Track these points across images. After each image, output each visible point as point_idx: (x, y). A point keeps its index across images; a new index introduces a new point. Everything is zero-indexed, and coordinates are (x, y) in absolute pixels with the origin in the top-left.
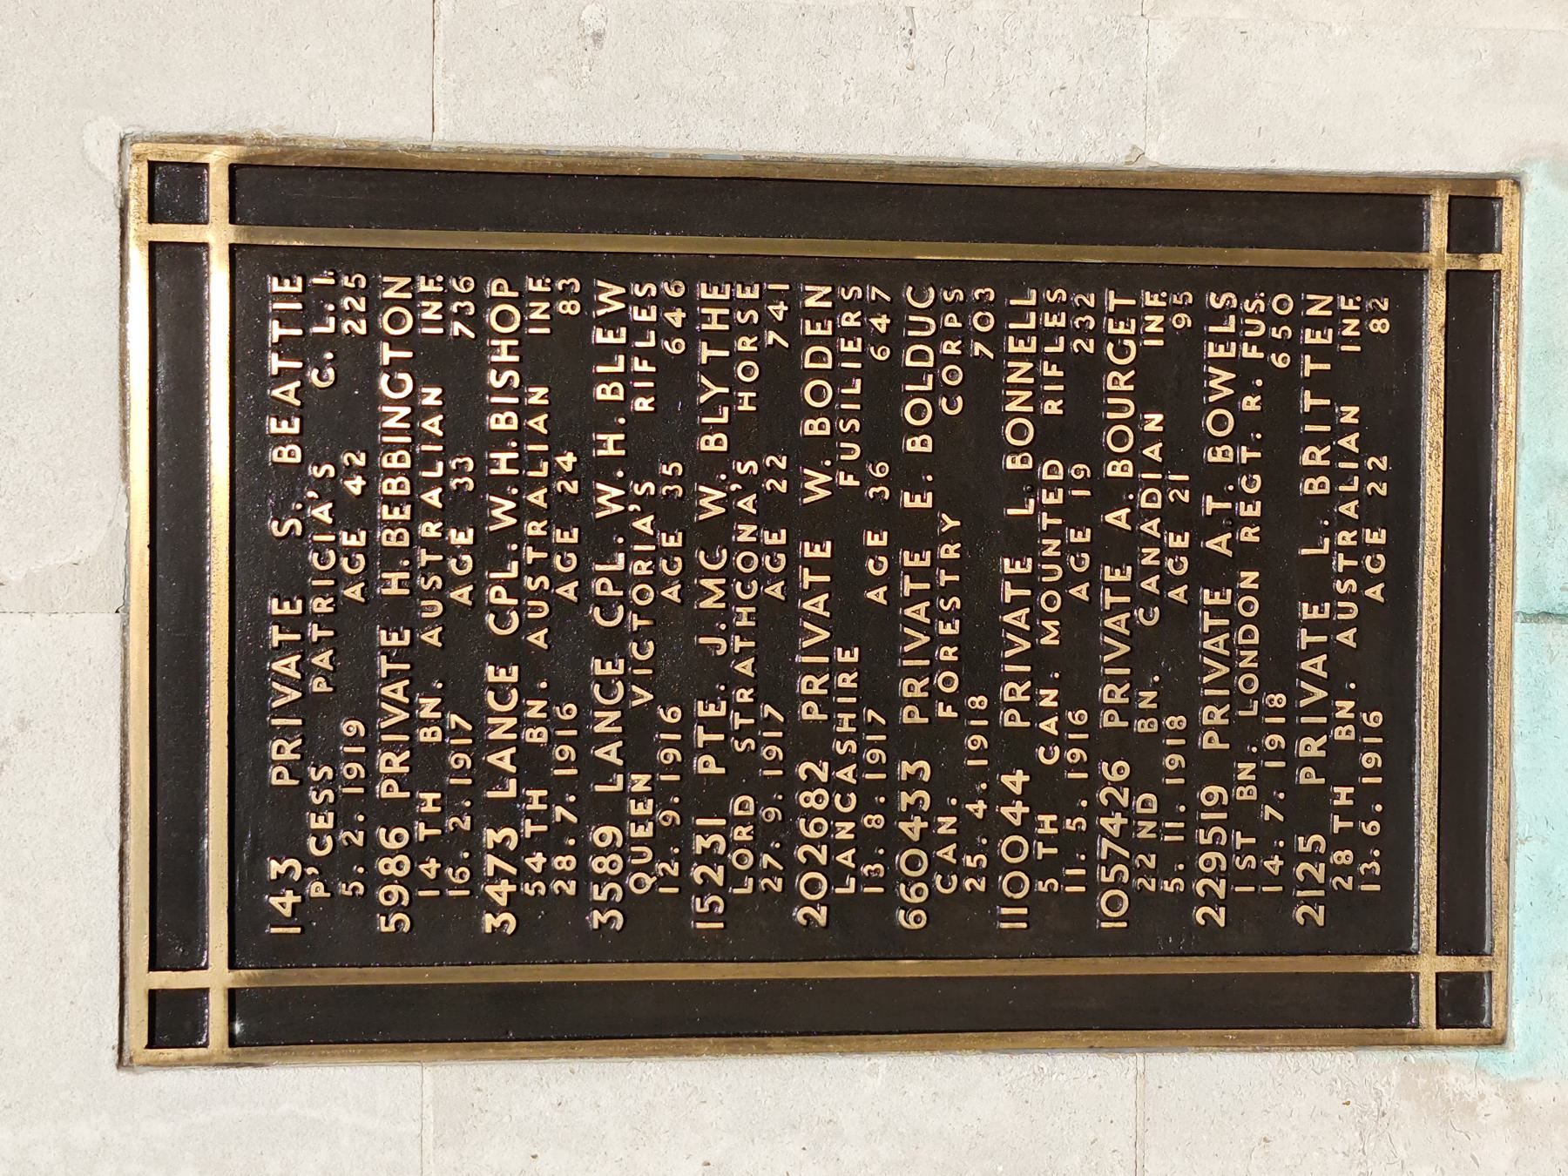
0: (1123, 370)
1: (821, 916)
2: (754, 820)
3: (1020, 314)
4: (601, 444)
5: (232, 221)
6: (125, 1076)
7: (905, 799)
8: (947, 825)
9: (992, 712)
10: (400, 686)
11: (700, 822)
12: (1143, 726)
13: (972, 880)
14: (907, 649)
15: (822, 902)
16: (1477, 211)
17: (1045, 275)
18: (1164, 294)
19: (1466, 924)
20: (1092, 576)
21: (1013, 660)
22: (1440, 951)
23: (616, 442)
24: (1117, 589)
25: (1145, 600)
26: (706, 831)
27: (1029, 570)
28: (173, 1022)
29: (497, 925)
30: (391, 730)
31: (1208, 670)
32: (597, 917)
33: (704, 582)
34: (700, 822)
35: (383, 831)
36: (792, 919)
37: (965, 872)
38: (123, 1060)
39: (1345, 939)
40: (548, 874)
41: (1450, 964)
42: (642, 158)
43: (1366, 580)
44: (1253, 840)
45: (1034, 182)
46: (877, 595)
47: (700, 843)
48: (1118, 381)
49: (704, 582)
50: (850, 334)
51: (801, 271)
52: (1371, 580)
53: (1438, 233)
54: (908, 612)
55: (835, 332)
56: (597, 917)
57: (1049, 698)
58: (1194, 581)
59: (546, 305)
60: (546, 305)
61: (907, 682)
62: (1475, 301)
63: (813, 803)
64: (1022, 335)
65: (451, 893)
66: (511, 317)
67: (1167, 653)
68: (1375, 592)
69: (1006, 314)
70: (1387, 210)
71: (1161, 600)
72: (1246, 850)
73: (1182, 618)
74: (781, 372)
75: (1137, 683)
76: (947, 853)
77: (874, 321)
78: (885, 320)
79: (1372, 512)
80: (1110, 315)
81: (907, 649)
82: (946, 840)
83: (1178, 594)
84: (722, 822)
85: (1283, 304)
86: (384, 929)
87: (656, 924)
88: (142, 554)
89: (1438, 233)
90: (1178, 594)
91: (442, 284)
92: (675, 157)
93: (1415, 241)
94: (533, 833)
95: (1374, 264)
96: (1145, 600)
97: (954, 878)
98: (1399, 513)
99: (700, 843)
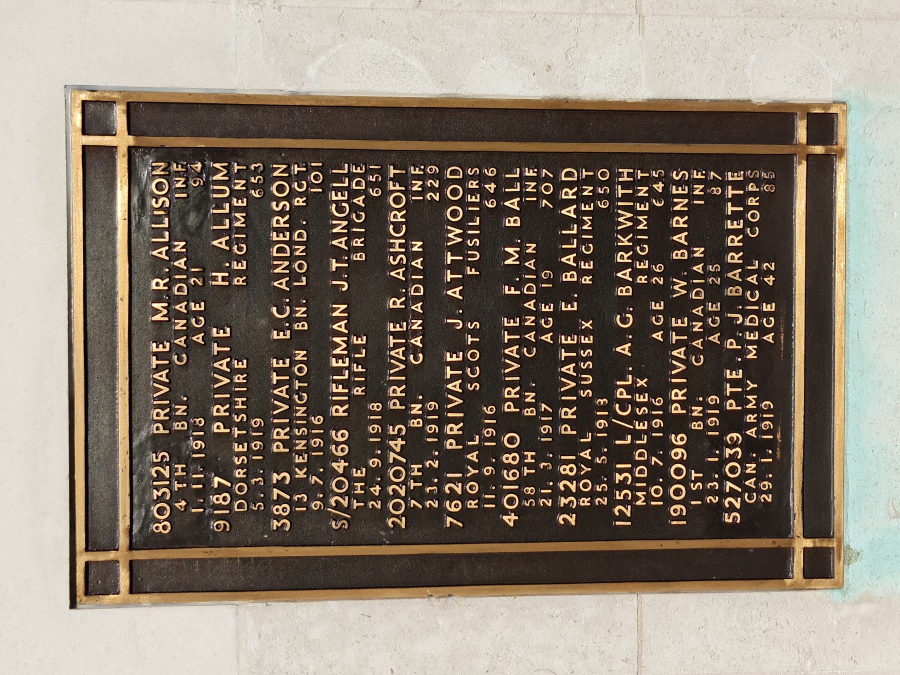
0: (399, 210)
1: (572, 520)
2: (646, 463)
3: (511, 183)
4: (215, 278)
5: (129, 134)
6: (73, 610)
7: (728, 452)
8: (751, 468)
9: (665, 407)
10: (164, 373)
11: (618, 466)
12: (529, 412)
13: (599, 499)
14: (674, 372)
15: (402, 515)
16: (824, 125)
17: (421, 158)
18: (422, 167)
19: (821, 516)
20: (205, 330)
21: (677, 376)
22: (805, 536)
23: (223, 277)
24: (679, 331)
25: (529, 344)
26: (621, 471)
27: (686, 325)
28: (90, 584)
29: (279, 525)
30: (452, 410)
31: (675, 367)
32: (275, 524)
33: (335, 339)
34: (618, 466)
35: (506, 471)
36: (557, 523)
37: (759, 492)
38: (73, 605)
39: (762, 526)
40: (537, 497)
41: (809, 543)
42: (577, 101)
43: (763, 331)
44: (701, 475)
45: (673, 108)
46: (658, 336)
47: (619, 477)
48: (397, 216)
49: (335, 339)
50: (472, 192)
51: (611, 161)
52: (766, 331)
53: (802, 134)
54: (506, 351)
55: (461, 195)
56: (275, 524)
57: (530, 397)
58: (556, 331)
59: (420, 183)
60: (420, 183)
61: (507, 389)
62: (822, 174)
63: (510, 461)
64: (337, 190)
65: (653, 503)
66: (685, 191)
67: (541, 372)
68: (769, 338)
69: (329, 179)
70: (774, 122)
71: (539, 343)
72: (697, 480)
73: (549, 352)
74: (660, 219)
75: (525, 388)
76: (750, 483)
77: (487, 186)
78: (493, 186)
79: (768, 294)
80: (391, 179)
81: (674, 372)
82: (750, 476)
83: (547, 338)
84: (630, 466)
85: (604, 175)
86: (727, 520)
87: (595, 522)
88: (124, 326)
89: (802, 134)
90: (714, 338)
91: (423, 170)
92: (769, 105)
93: (788, 136)
94: (528, 474)
95: (756, 166)
96: (529, 344)
97: (755, 494)
98: (781, 293)
99: (619, 477)
